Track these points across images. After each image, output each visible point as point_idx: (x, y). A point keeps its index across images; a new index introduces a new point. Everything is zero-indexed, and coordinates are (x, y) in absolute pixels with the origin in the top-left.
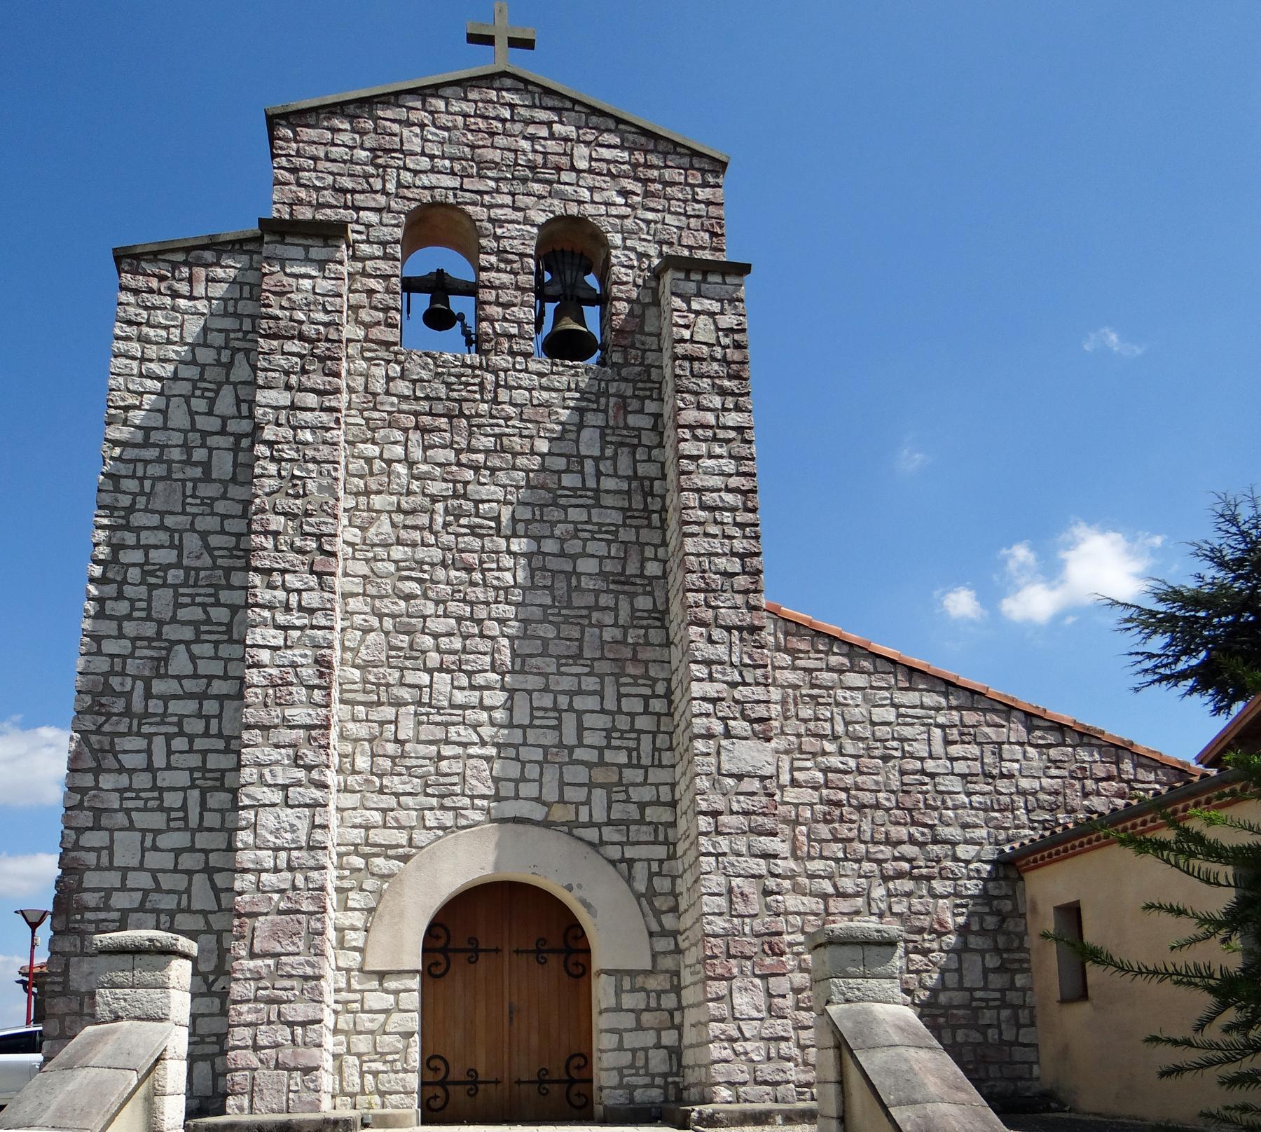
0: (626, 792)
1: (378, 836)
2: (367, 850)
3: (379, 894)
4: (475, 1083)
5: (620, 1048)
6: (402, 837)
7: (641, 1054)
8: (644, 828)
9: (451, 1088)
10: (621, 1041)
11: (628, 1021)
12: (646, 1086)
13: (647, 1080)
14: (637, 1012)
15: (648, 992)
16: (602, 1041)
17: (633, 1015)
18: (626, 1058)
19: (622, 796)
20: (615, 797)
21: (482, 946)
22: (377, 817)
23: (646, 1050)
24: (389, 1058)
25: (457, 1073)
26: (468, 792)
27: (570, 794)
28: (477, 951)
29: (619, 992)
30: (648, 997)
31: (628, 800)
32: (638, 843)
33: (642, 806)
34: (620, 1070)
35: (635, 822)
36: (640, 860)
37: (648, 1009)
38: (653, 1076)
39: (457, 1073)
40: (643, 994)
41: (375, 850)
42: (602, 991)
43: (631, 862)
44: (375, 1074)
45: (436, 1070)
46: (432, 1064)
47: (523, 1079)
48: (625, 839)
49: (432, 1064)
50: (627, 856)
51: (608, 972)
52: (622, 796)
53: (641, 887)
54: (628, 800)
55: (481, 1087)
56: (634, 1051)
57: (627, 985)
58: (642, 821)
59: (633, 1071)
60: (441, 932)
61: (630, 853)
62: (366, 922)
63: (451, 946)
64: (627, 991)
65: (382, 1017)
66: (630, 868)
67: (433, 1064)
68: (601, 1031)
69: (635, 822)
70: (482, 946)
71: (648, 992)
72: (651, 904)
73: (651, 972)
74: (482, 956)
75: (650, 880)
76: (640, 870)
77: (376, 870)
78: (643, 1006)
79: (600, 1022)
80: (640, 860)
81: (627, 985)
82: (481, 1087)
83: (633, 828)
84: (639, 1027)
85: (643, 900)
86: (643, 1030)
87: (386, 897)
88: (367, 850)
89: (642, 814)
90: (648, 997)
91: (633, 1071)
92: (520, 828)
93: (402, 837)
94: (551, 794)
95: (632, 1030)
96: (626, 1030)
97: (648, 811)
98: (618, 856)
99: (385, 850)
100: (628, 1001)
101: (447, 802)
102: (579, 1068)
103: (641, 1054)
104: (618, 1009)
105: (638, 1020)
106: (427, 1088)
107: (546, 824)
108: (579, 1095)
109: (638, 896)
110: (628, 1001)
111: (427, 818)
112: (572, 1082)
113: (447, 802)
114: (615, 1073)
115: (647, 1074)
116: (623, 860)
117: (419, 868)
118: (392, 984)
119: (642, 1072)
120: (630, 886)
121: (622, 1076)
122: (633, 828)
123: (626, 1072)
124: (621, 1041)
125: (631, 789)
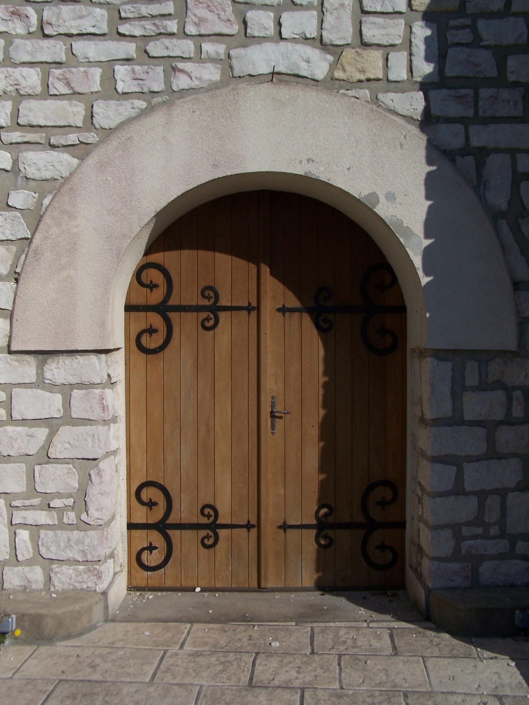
0: (474, 30)
1: (36, 112)
2: (16, 136)
3: (35, 218)
4: (214, 527)
5: (458, 490)
6: (75, 113)
7: (493, 501)
8: (505, 94)
9: (174, 534)
10: (459, 478)
11: (472, 442)
12: (501, 557)
13: (503, 545)
14: (489, 426)
15: (508, 390)
16: (424, 475)
17: (481, 432)
18: (466, 509)
19: (465, 36)
20: (452, 37)
21: (224, 302)
22: (32, 79)
23: (502, 493)
24: (56, 503)
25: (184, 510)
26: (191, 29)
27: (373, 31)
28: (216, 309)
29: (458, 388)
30: (510, 399)
31: (476, 42)
32: (494, 120)
33: (501, 53)
34: (456, 529)
35: (488, 82)
36: (497, 151)
37: (508, 421)
38: (513, 539)
39: (184, 510)
40: (499, 395)
41: (30, 137)
42: (425, 385)
43: (481, 154)
44: (35, 529)
45: (151, 504)
46: (145, 495)
47: (291, 522)
48: (470, 113)
49: (145, 495)
50: (475, 142)
51: (440, 355)
52: (465, 36)
53: (500, 199)
54: (476, 42)
55: (223, 533)
56: (482, 496)
57: (472, 378)
58: (500, 81)
59: (479, 531)
60: (155, 276)
61: (480, 137)
62: (15, 264)
63: (172, 302)
64: (473, 389)
65: (42, 433)
66: (480, 165)
67: (147, 494)
68: (422, 354)
69: (488, 82)
70: (224, 302)
71: (508, 390)
72: (516, 230)
73: (515, 354)
74: (223, 316)
75: (515, 186)
76: (497, 167)
77: (31, 172)
78: (500, 416)
79: (422, 439)
80: (497, 151)
81: (472, 378)
82: (223, 533)
83: (485, 93)
84: (493, 454)
85: (504, 225)
86: (500, 457)
87: (47, 220)
88: (16, 136)
89: (502, 67)
90: (510, 399)
91: (479, 531)
92: (283, 92)
93: (75, 113)
94: (339, 29)
95: (478, 459)
96: (470, 459)
97: (512, 62)
98: (457, 143)
99: (48, 138)
100: (474, 406)
101: (156, 49)
102: (383, 503)
103: (493, 501)
104: (456, 420)
105: (491, 440)
106: (137, 533)
107: (332, 84)
108: (382, 547)
109: (496, 216)
110: (474, 406)
111: (118, 76)
112: (371, 526)
113: (156, 49)
114: (448, 533)
115: (502, 535)
116: (467, 150)
117: (102, 166)
118: (58, 371)
119: (494, 531)
120: (482, 199)
121: (459, 538)
122: (485, 93)
123: (466, 531)
124: (459, 478)
125: (481, 24)
